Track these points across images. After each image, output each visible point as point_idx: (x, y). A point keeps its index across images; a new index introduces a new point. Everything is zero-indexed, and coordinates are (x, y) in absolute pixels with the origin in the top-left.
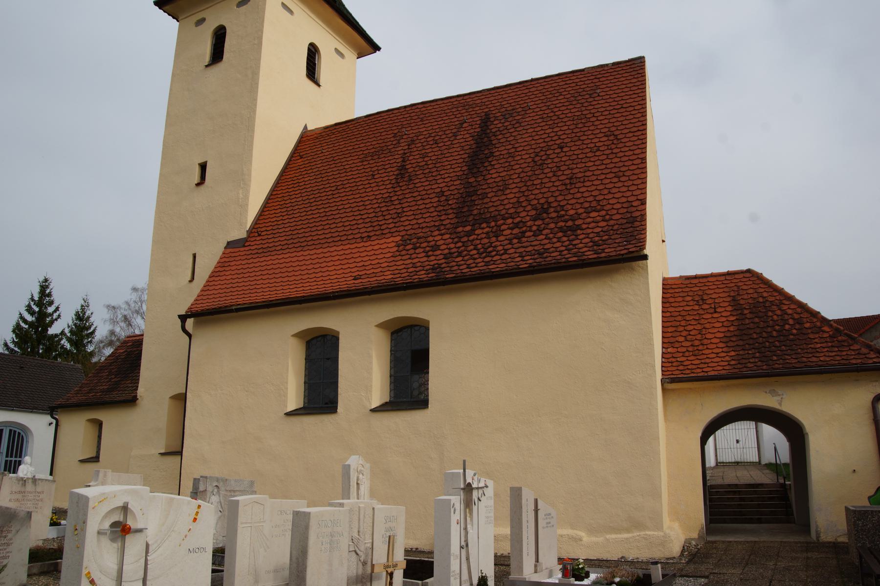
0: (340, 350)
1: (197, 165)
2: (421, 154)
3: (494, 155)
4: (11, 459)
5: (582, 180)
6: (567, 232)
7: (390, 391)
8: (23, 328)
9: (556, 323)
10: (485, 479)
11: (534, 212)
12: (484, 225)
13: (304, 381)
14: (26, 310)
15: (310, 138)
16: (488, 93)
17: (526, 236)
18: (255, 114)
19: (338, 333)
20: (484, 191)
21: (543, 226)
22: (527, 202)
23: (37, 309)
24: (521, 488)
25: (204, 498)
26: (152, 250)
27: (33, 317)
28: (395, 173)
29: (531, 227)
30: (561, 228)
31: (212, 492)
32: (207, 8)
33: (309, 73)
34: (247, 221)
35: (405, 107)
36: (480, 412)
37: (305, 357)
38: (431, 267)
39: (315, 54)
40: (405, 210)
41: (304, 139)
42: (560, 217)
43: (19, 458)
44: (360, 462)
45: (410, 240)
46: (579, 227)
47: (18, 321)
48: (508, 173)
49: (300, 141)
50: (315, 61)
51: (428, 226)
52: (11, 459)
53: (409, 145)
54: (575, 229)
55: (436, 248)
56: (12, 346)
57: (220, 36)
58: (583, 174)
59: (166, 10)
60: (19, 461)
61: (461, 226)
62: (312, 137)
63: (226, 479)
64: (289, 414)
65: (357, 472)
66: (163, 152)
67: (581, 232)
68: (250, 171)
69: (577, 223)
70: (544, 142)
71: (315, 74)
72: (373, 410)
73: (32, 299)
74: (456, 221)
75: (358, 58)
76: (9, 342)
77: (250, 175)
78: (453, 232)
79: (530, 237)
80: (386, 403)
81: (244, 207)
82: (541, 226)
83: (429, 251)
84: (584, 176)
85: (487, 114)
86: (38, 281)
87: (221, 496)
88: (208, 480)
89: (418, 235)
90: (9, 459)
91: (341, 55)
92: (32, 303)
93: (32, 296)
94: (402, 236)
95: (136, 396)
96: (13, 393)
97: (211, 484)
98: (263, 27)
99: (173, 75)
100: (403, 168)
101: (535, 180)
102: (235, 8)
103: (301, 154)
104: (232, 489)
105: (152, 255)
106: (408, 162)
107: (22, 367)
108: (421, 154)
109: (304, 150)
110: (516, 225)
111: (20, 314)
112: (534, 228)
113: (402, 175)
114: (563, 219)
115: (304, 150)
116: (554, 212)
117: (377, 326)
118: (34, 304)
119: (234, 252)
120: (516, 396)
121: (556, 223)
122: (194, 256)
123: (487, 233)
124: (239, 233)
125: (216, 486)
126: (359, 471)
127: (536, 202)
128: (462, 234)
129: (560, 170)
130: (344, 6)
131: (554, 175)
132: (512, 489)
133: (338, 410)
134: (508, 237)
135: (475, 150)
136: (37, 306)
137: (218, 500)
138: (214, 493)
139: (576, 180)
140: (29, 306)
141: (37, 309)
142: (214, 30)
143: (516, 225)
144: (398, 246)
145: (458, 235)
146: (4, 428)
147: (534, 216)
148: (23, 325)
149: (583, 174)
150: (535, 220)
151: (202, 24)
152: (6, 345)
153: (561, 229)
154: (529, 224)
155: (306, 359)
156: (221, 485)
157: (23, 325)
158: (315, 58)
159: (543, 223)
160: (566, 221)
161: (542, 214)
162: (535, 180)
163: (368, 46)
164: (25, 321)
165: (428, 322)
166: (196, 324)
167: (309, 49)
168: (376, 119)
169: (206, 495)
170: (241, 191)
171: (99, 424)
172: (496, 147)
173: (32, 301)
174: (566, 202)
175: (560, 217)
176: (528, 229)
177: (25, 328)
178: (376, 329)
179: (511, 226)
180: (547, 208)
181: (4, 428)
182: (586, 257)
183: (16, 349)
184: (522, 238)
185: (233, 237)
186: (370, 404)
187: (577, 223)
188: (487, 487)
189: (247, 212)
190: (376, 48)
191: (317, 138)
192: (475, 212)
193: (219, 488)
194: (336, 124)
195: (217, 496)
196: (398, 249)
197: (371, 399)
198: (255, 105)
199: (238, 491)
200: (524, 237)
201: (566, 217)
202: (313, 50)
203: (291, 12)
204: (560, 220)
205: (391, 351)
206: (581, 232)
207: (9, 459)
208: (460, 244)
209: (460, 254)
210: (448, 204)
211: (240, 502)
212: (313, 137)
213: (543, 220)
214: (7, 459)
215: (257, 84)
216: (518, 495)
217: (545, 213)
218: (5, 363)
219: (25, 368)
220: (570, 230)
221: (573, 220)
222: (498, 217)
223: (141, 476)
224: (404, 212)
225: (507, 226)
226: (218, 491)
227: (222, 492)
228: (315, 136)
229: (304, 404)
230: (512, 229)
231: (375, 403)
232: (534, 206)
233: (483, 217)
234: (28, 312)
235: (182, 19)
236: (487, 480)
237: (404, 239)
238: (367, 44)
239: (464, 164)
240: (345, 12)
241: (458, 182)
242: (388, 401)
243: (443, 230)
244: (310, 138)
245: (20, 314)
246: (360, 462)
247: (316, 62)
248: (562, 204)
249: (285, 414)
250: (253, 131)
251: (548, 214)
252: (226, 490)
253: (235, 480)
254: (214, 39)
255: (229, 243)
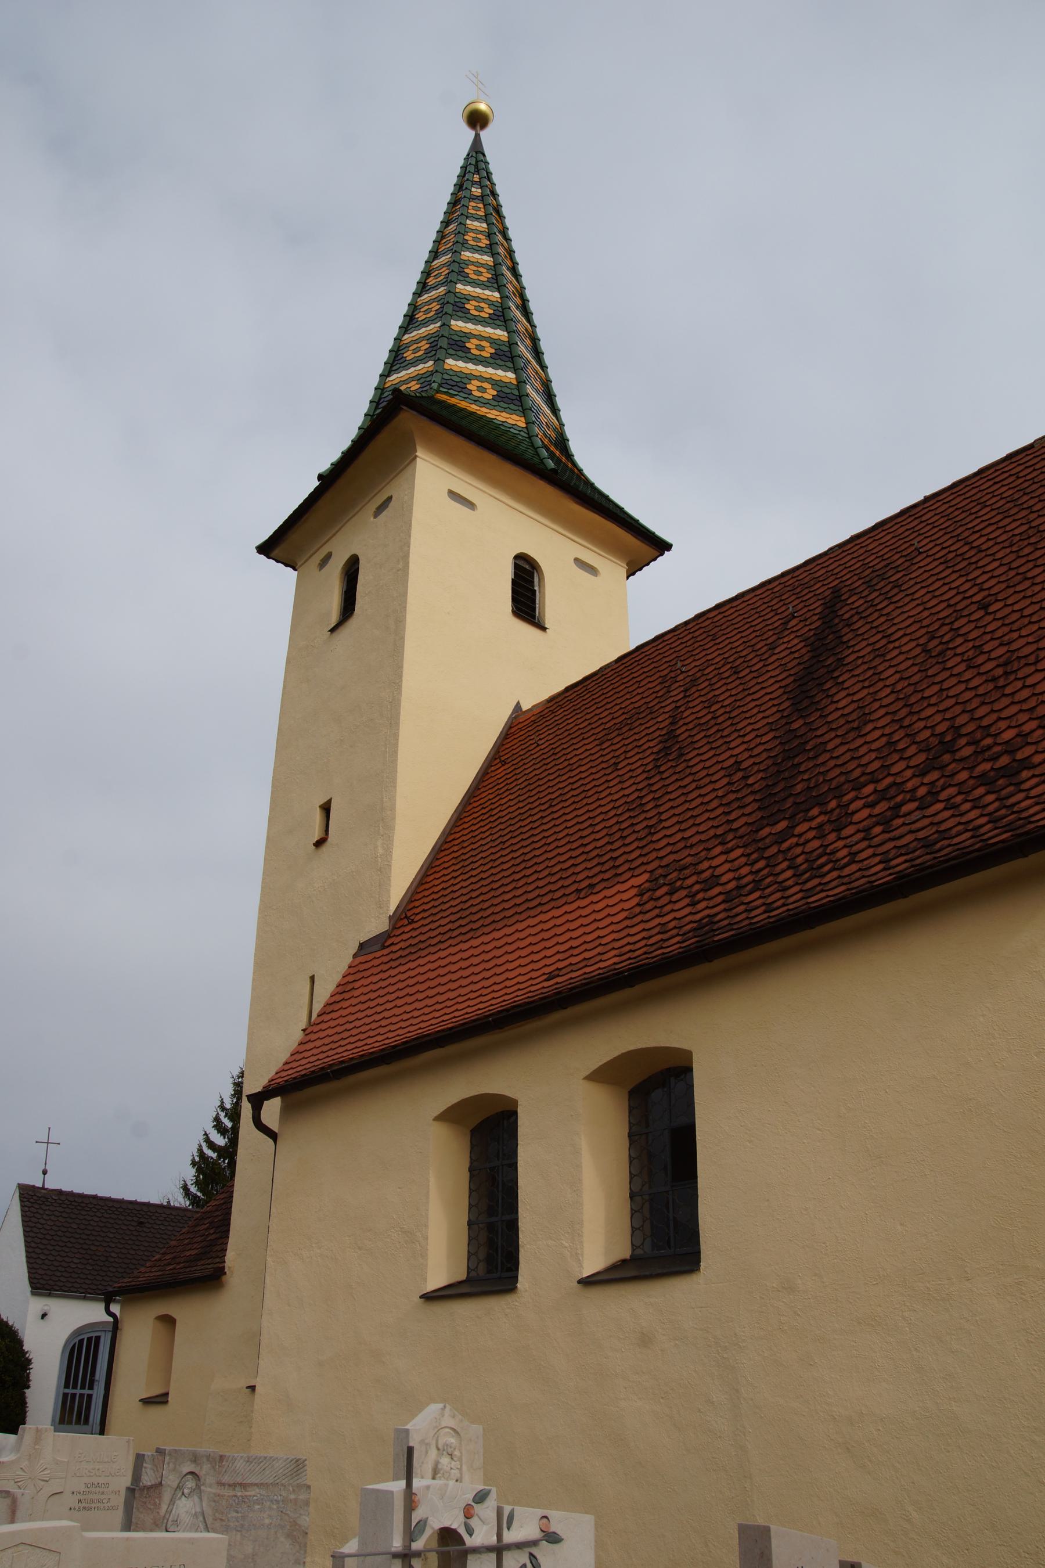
0: (519, 1142)
1: (318, 809)
2: (706, 701)
3: (845, 663)
4: (74, 1391)
5: (1032, 659)
6: (996, 781)
7: (633, 1232)
8: (209, 1157)
9: (983, 1015)
10: (545, 1512)
11: (922, 757)
12: (815, 811)
13: (467, 1219)
14: (213, 1127)
15: (523, 725)
16: (841, 551)
17: (901, 814)
18: (400, 693)
19: (515, 1102)
20: (819, 740)
21: (942, 781)
22: (909, 740)
23: (229, 1124)
24: (766, 1530)
25: (155, 1504)
26: (254, 980)
27: (224, 1138)
28: (655, 750)
29: (914, 790)
30: (984, 774)
31: (179, 1487)
32: (334, 535)
33: (516, 607)
34: (390, 897)
35: (686, 623)
36: (816, 1275)
37: (467, 1165)
38: (695, 925)
39: (533, 573)
40: (663, 817)
41: (513, 730)
42: (983, 751)
43: (89, 1389)
44: (448, 1421)
45: (665, 876)
46: (1026, 764)
47: (200, 1146)
48: (871, 690)
49: (507, 735)
50: (533, 586)
51: (702, 839)
52: (74, 1391)
53: (686, 691)
54: (1010, 773)
55: (713, 881)
56: (193, 1189)
57: (351, 572)
58: (1034, 647)
59: (279, 559)
60: (88, 1395)
61: (768, 825)
62: (527, 722)
63: (221, 1456)
64: (430, 1297)
65: (438, 1449)
66: (271, 798)
67: (1030, 773)
68: (393, 799)
69: (1019, 756)
70: (949, 606)
71: (534, 609)
72: (588, 1282)
73: (222, 1107)
74: (760, 816)
75: (630, 574)
76: (189, 1183)
77: (393, 809)
78: (750, 840)
79: (909, 813)
80: (624, 1261)
81: (383, 870)
82: (937, 784)
83: (698, 892)
84: (1038, 649)
85: (836, 592)
86: (231, 1076)
87: (205, 1498)
88: (167, 1458)
89: (682, 862)
90: (86, 1392)
91: (592, 570)
92: (222, 1115)
93: (222, 1102)
94: (651, 872)
95: (224, 1268)
96: (119, 1270)
97: (174, 1469)
98: (410, 536)
99: (288, 662)
100: (671, 735)
101: (927, 687)
102: (372, 519)
103: (503, 759)
104: (239, 1480)
105: (254, 989)
106: (681, 723)
107: (142, 1223)
108: (706, 701)
109: (511, 749)
110: (882, 795)
111: (206, 1134)
112: (922, 791)
113: (666, 751)
114: (987, 755)
115: (511, 749)
116: (968, 744)
117: (590, 1078)
118: (225, 1117)
119: (366, 962)
120: (901, 1224)
121: (972, 768)
122: (312, 978)
123: (820, 826)
124: (377, 925)
125: (192, 1473)
126: (440, 1446)
127: (927, 733)
128: (767, 841)
129: (982, 653)
130: (592, 485)
131: (969, 668)
132: (743, 1529)
133: (518, 1285)
134: (861, 826)
135: (808, 664)
136: (231, 1119)
137: (198, 1510)
138: (186, 1491)
139: (1019, 662)
140: (217, 1119)
141: (229, 1124)
142: (343, 568)
143: (882, 795)
144: (641, 895)
145: (760, 845)
146: (102, 1334)
147: (922, 766)
148: (210, 1153)
149: (1034, 647)
150: (924, 774)
151: (327, 563)
152: (185, 1188)
153: (983, 779)
154: (909, 785)
155: (470, 1170)
156: (204, 1470)
157: (210, 1153)
158: (533, 582)
159: (943, 776)
160: (995, 758)
161: (940, 756)
162: (927, 687)
163: (643, 545)
164: (211, 1145)
165: (688, 1055)
166: (286, 1111)
167: (517, 567)
168: (633, 660)
169: (160, 1497)
170: (379, 843)
171: (169, 1321)
172: (849, 647)
173: (223, 1111)
174: (994, 717)
175: (983, 751)
176: (908, 796)
177: (212, 1158)
178: (591, 1087)
179: (870, 799)
180: (953, 740)
181: (102, 1334)
182: (1032, 826)
183: (199, 1194)
184: (892, 820)
185: (369, 932)
186: (581, 1266)
187: (1019, 756)
188: (553, 1538)
189: (390, 880)
190: (662, 546)
191: (534, 722)
192: (799, 788)
193: (199, 1480)
194: (567, 689)
195: (196, 1498)
196: (641, 900)
197: (582, 1255)
198: (400, 677)
199: (256, 1485)
200: (898, 817)
201: (996, 749)
202: (527, 567)
203: (471, 505)
204: (980, 759)
205: (630, 1135)
206: (1030, 773)
207: (86, 1392)
208: (761, 864)
209: (757, 885)
210: (747, 784)
211: (119, 1526)
212: (529, 721)
213: (942, 768)
214: (90, 1392)
215: (403, 638)
216: (762, 1554)
217: (948, 752)
218: (113, 1216)
219: (147, 1225)
220: (1003, 777)
221: (1012, 752)
222: (846, 786)
223: (128, 1441)
224: (661, 821)
225: (863, 801)
226: (198, 1487)
227: (210, 1489)
228: (532, 719)
229: (468, 1273)
230: (872, 805)
231: (593, 1263)
232: (923, 745)
233: (814, 794)
234: (217, 1130)
235: (300, 566)
236: (552, 1514)
237: (653, 877)
238: (641, 541)
239: (785, 697)
240: (611, 507)
241: (771, 735)
242: (628, 1257)
243: (731, 840)
244: (523, 725)
245: (206, 1134)
246: (448, 1421)
247: (536, 588)
248: (985, 722)
249: (421, 1297)
250: (397, 724)
251: (954, 752)
252: (221, 1484)
253: (249, 1458)
254: (345, 583)
255: (362, 946)
